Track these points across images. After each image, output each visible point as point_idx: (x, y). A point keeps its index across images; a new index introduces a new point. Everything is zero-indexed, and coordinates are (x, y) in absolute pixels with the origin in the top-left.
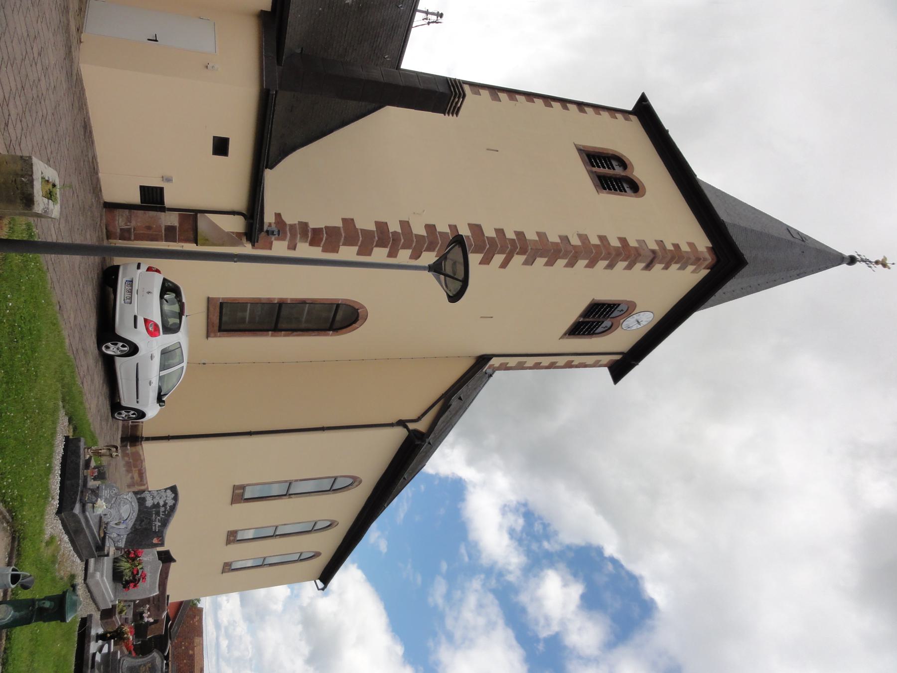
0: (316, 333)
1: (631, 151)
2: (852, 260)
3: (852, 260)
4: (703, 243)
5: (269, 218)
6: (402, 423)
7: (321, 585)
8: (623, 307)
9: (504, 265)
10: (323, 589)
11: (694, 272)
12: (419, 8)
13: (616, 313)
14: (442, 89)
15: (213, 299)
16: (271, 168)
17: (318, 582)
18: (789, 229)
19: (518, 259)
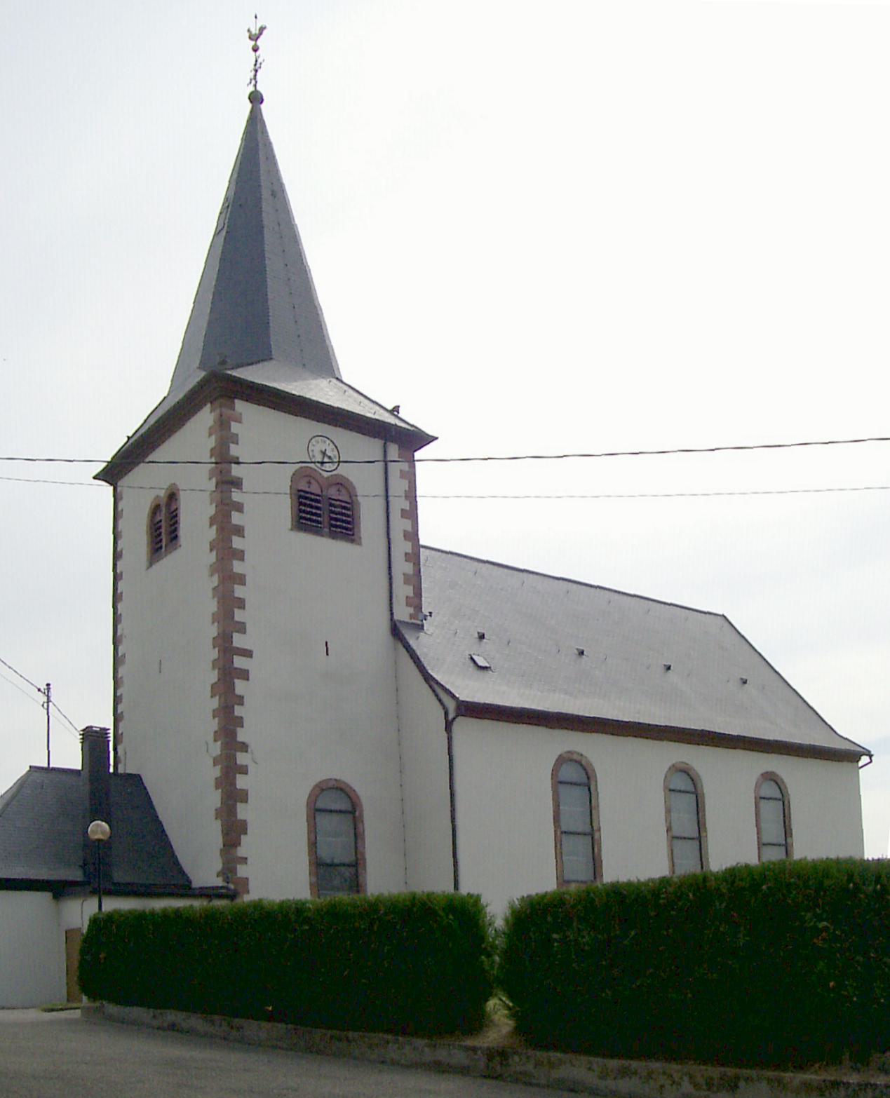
0: (360, 825)
1: (161, 488)
2: (256, 99)
3: (256, 99)
4: (205, 417)
5: (219, 882)
6: (449, 726)
7: (865, 759)
8: (303, 486)
9: (248, 654)
10: (871, 756)
11: (239, 421)
12: (46, 765)
13: (315, 489)
14: (87, 743)
15: (72, 930)
16: (191, 882)
17: (860, 764)
18: (217, 234)
19: (238, 641)
